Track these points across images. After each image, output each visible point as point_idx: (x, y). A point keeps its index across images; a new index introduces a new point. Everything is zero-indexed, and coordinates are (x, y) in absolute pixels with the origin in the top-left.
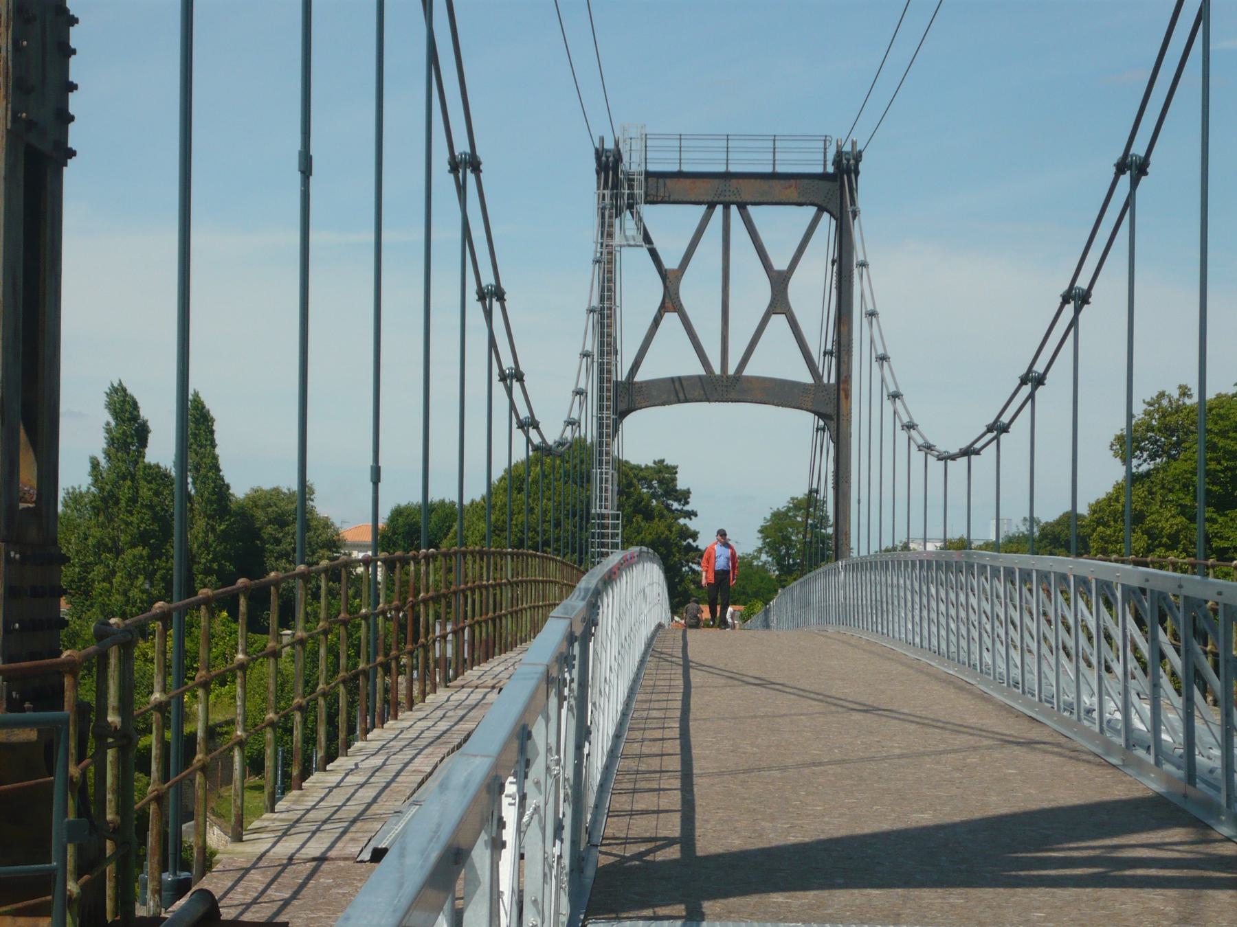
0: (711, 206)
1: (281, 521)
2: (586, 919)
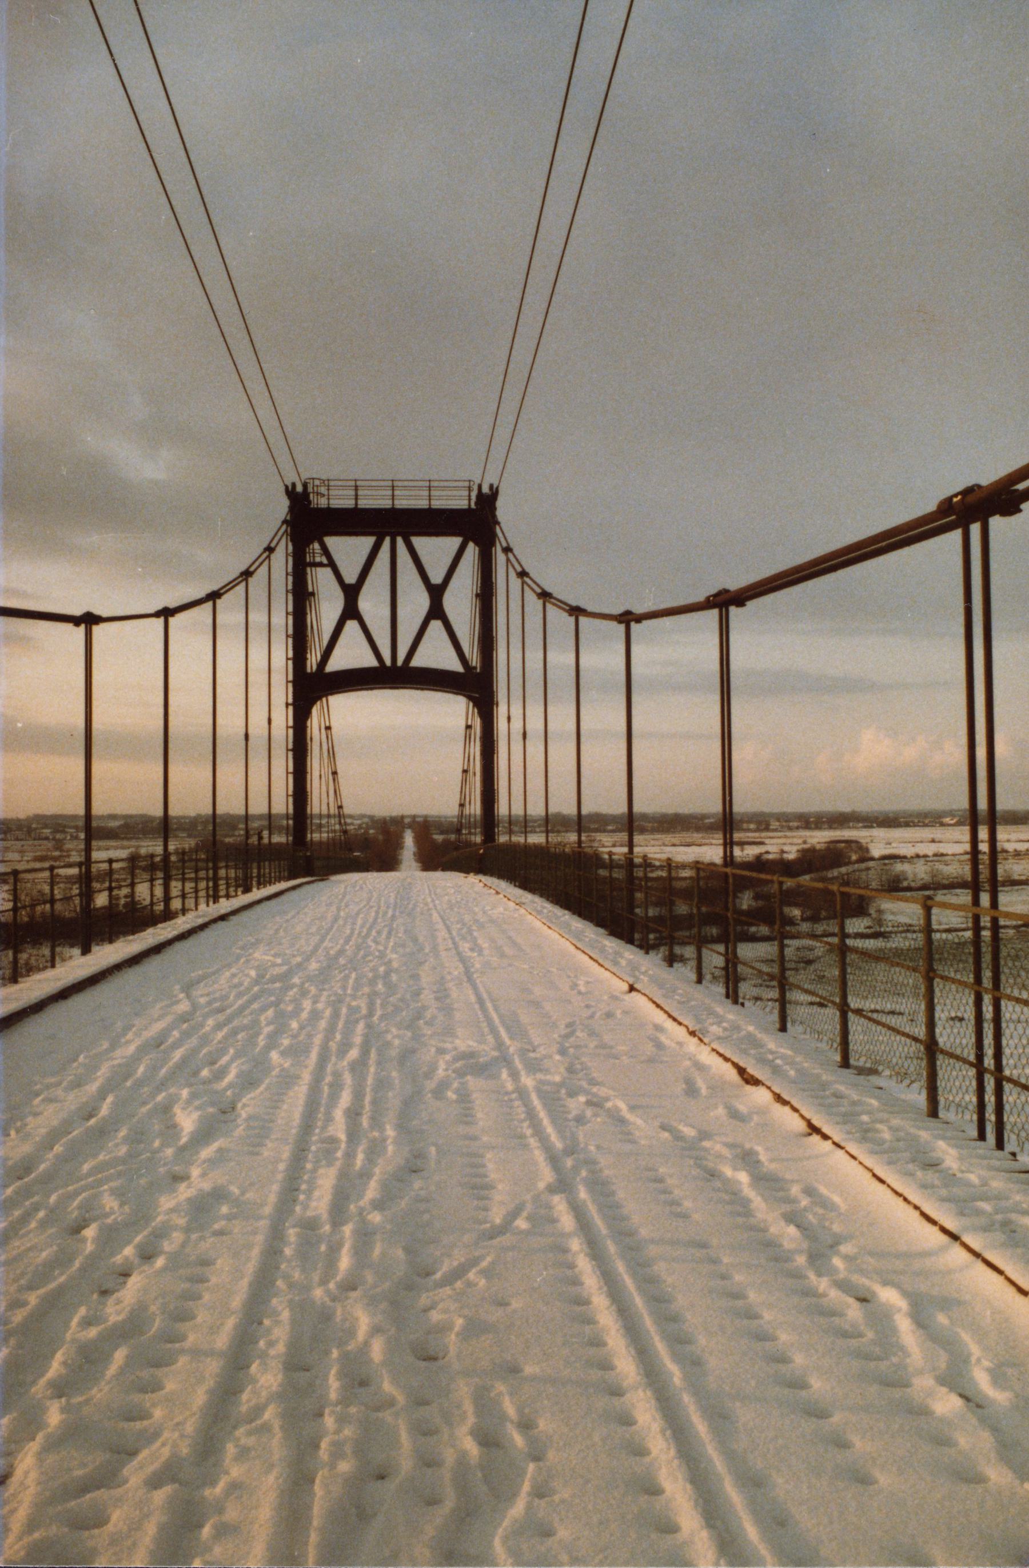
2: (872, 859)
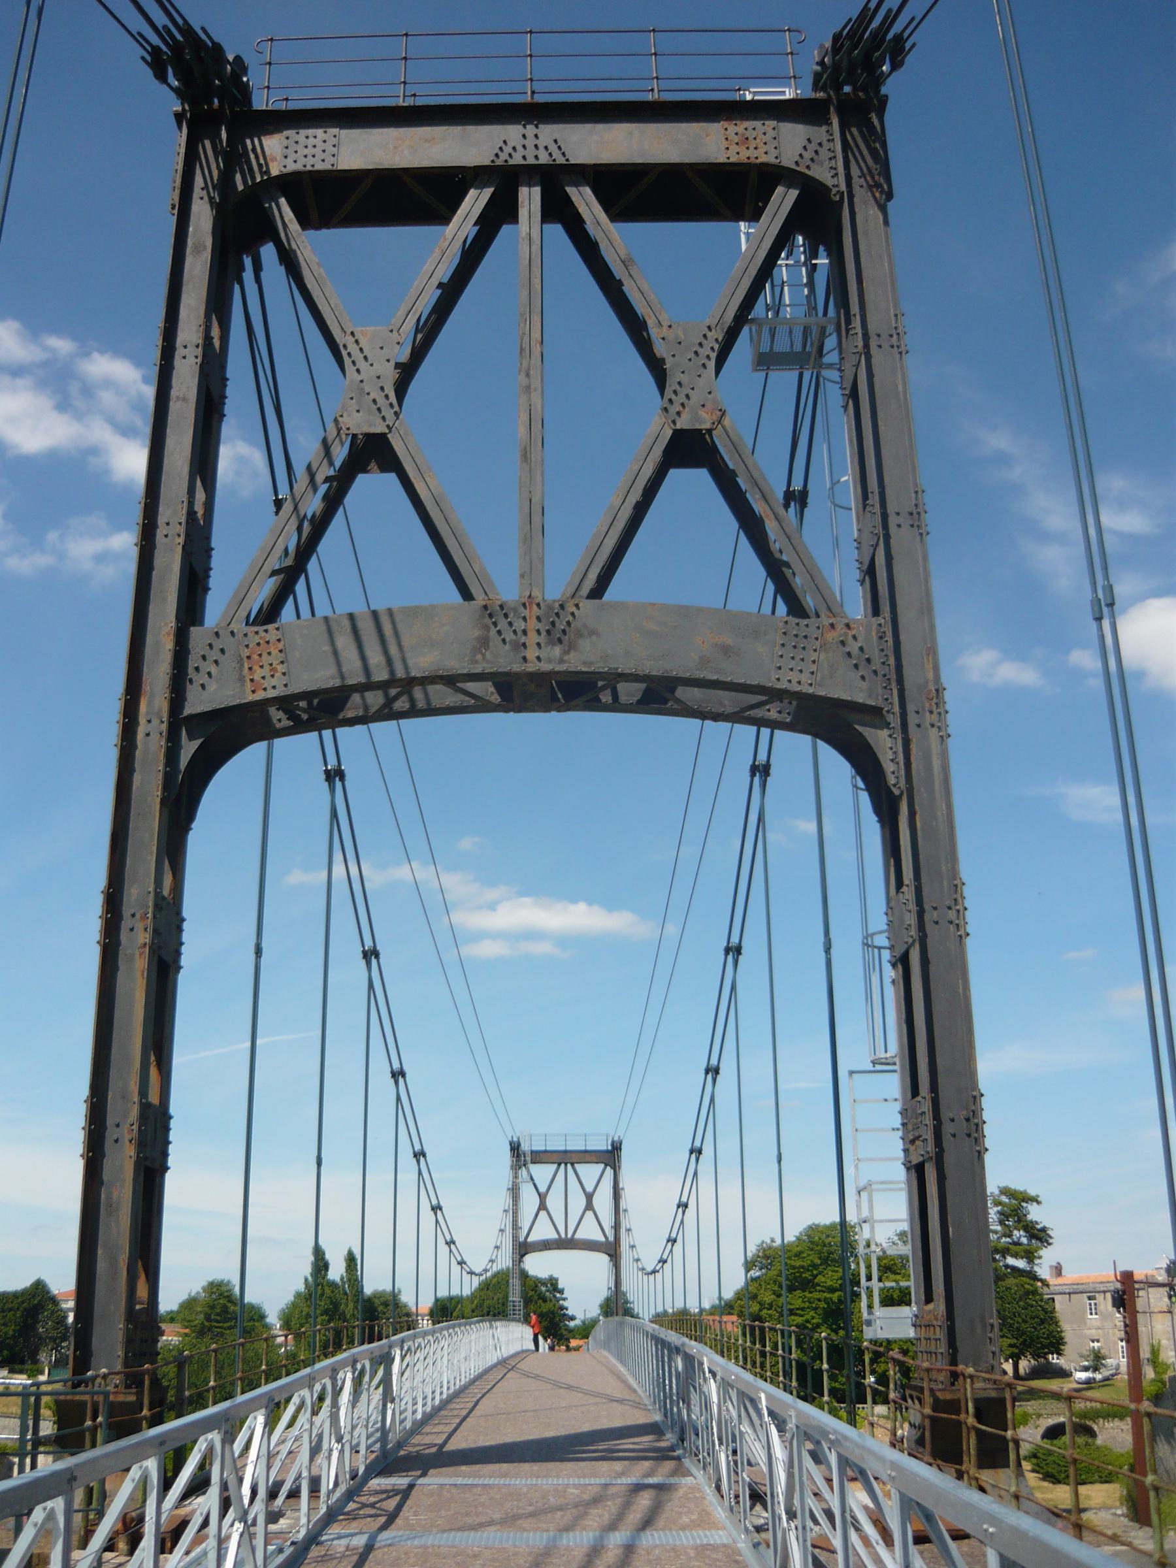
0: (559, 1164)
1: (386, 1304)
